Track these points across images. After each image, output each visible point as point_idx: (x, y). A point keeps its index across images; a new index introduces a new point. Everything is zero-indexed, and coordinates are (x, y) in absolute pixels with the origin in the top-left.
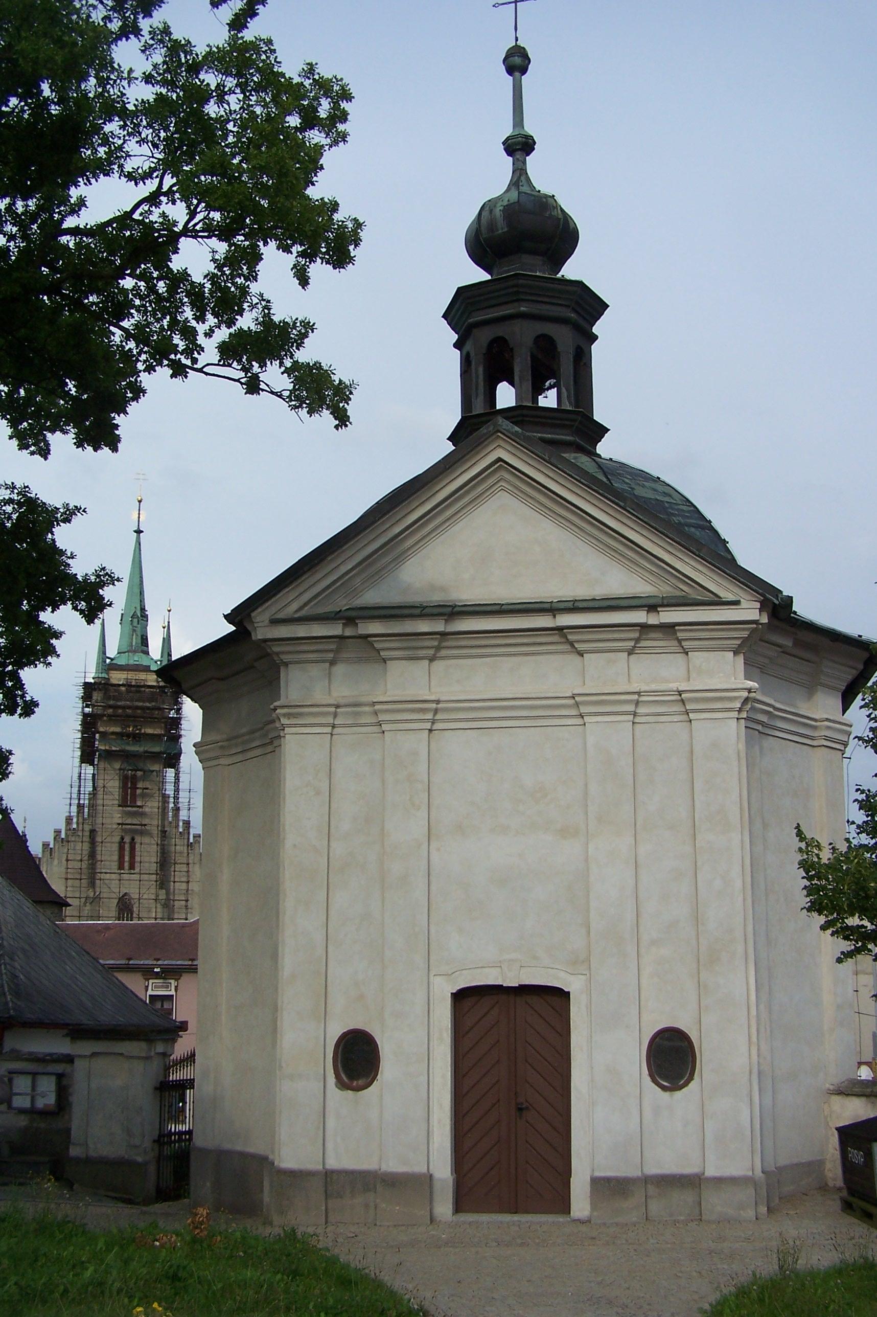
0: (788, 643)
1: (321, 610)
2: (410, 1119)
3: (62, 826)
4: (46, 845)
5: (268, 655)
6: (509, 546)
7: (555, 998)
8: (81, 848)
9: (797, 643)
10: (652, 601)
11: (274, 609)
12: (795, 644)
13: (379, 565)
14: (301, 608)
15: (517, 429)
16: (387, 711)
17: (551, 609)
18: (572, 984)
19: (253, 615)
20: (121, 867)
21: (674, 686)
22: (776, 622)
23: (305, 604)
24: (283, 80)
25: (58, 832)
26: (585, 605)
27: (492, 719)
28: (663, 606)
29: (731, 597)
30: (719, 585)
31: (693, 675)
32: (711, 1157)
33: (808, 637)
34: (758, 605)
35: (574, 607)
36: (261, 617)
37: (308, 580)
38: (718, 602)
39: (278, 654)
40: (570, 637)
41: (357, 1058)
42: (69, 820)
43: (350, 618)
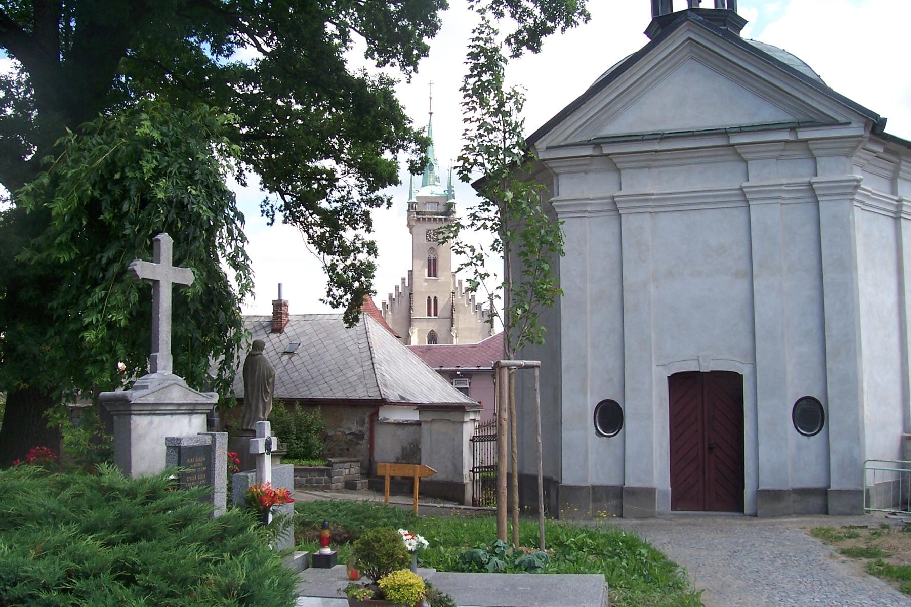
0: (879, 149)
1: (578, 140)
2: (648, 451)
3: (393, 291)
4: (384, 304)
5: (545, 169)
6: (689, 99)
7: (735, 379)
8: (405, 302)
9: (886, 151)
10: (792, 125)
11: (549, 140)
12: (884, 151)
13: (613, 110)
14: (566, 139)
15: (701, 18)
16: (625, 202)
17: (725, 132)
18: (744, 371)
19: (536, 144)
20: (429, 314)
21: (807, 180)
22: (874, 137)
23: (569, 136)
24: (73, 24)
25: (390, 296)
26: (747, 129)
27: (689, 204)
28: (800, 127)
29: (843, 120)
30: (836, 112)
31: (819, 172)
32: (834, 476)
33: (892, 146)
34: (863, 125)
35: (741, 130)
36: (541, 145)
37: (569, 121)
38: (835, 123)
39: (551, 168)
40: (739, 151)
41: (610, 416)
42: (397, 288)
43: (597, 143)
